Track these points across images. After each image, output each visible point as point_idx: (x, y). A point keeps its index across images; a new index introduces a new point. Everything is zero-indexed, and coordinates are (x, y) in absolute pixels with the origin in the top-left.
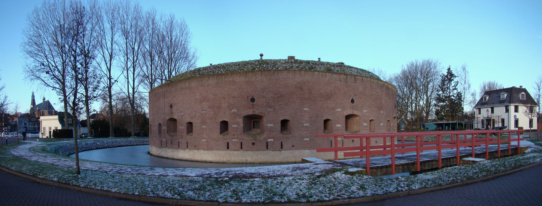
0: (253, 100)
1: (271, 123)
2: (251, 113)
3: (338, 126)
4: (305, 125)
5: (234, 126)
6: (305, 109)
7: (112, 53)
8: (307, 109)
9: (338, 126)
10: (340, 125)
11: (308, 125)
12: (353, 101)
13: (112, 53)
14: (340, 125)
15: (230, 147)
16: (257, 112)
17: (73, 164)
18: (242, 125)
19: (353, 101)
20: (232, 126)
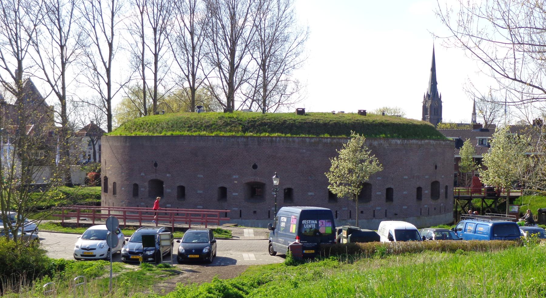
0: (156, 165)
1: (170, 190)
2: (253, 180)
3: (234, 194)
4: (199, 192)
5: (142, 189)
6: (198, 176)
7: (100, 90)
8: (202, 176)
9: (234, 194)
10: (237, 194)
11: (201, 192)
12: (255, 167)
13: (100, 90)
14: (237, 194)
15: (242, 216)
16: (258, 179)
17: (175, 225)
18: (148, 189)
19: (255, 167)
20: (233, 194)
